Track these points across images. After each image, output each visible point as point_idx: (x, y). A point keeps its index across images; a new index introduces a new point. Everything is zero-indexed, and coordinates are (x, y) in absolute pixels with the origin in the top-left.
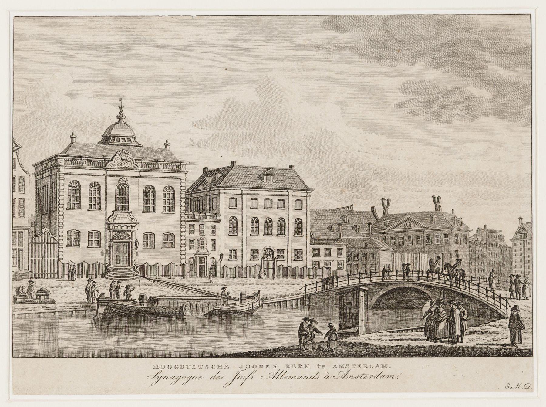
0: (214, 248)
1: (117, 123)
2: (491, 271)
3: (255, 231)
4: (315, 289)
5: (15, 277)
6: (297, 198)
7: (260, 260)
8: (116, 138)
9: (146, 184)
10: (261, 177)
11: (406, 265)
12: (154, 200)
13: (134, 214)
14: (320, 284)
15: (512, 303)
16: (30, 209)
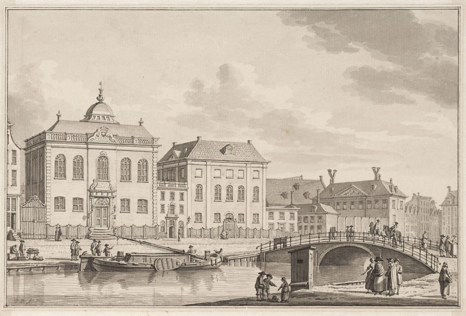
0: (182, 211)
1: (97, 104)
2: (424, 233)
3: (218, 197)
4: (269, 248)
5: (9, 237)
6: (241, 169)
7: (222, 222)
8: (96, 116)
9: (123, 157)
10: (223, 151)
11: (349, 227)
12: (65, 170)
13: (113, 183)
14: (272, 244)
15: (442, 260)
16: (21, 178)
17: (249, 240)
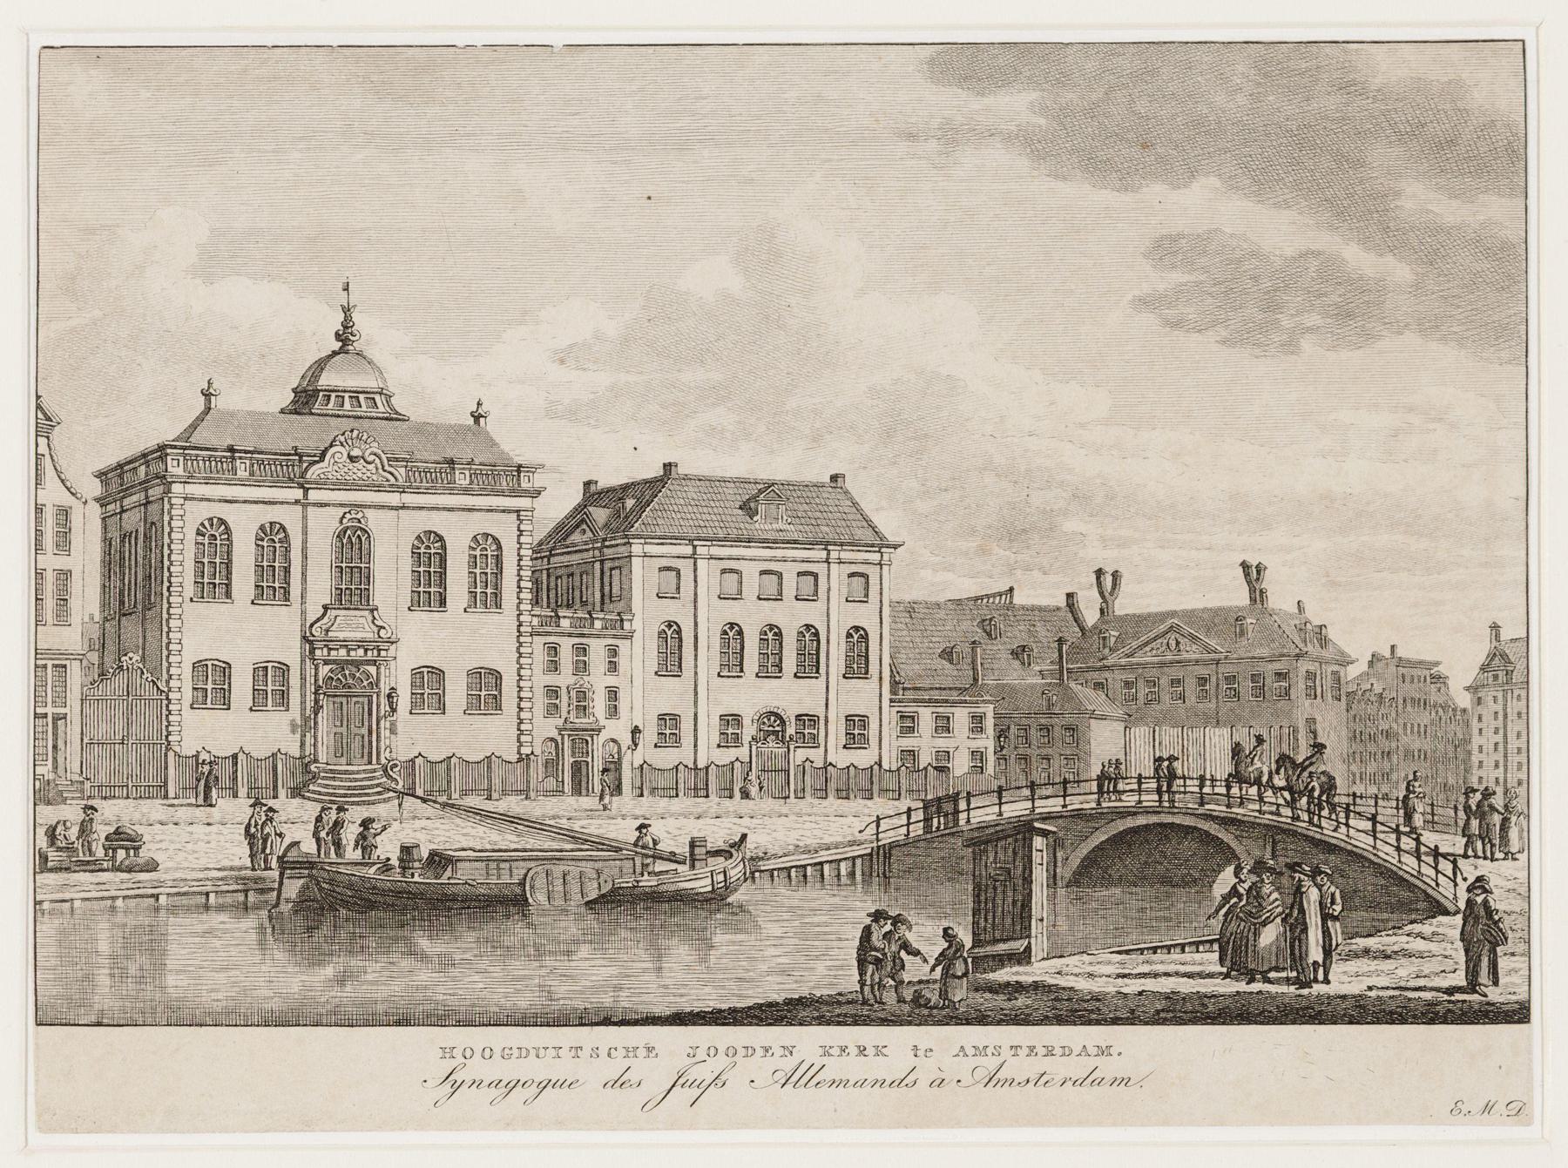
0: (613, 712)
1: (335, 353)
3: (733, 664)
4: (904, 830)
5: (43, 794)
6: (854, 568)
7: (747, 746)
8: (333, 395)
9: (421, 528)
10: (748, 508)
11: (1165, 760)
13: (386, 615)
14: (918, 815)
16: (87, 599)
17: (832, 803)
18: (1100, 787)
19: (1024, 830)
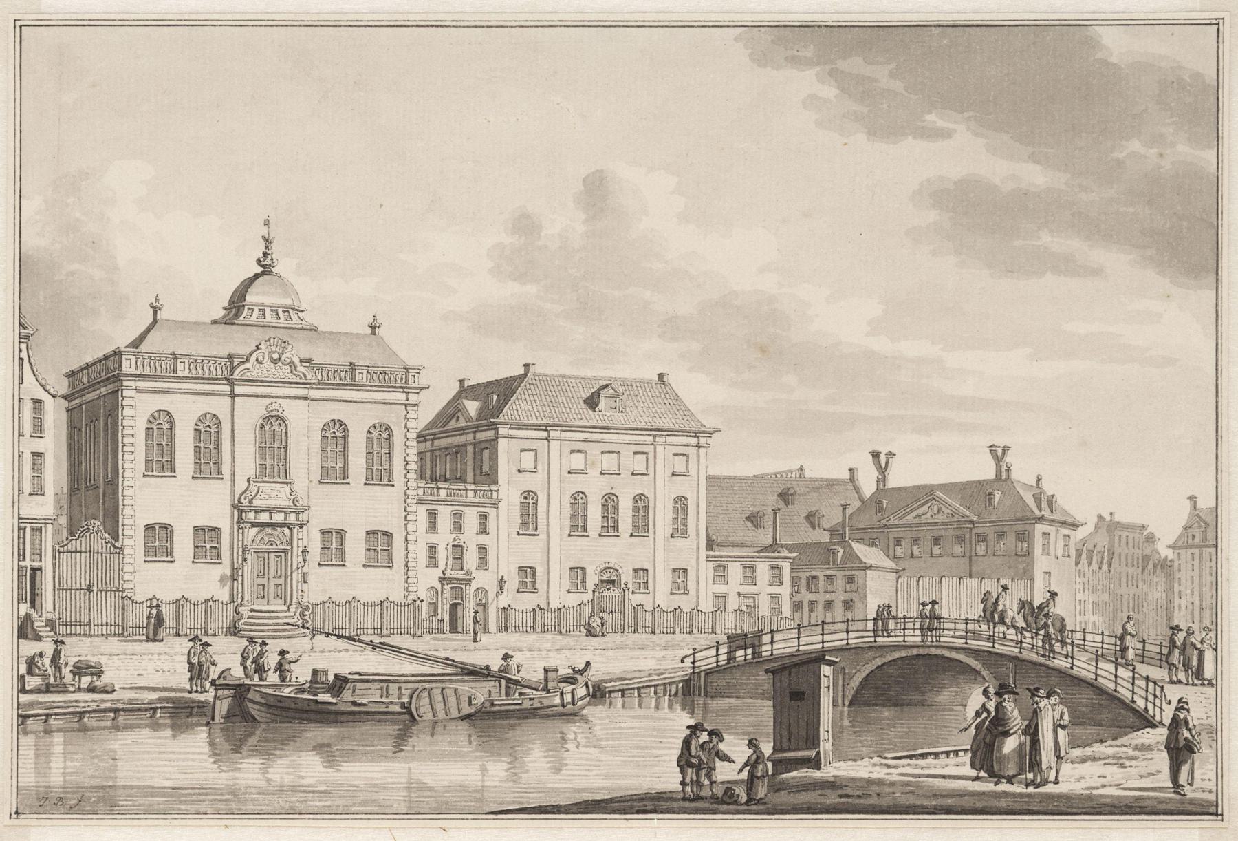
0: (483, 562)
1: (257, 276)
3: (579, 525)
4: (714, 659)
5: (25, 630)
7: (590, 592)
8: (256, 309)
9: (328, 417)
10: (592, 402)
11: (928, 605)
13: (300, 486)
15: (1173, 693)
16: (55, 474)
18: (875, 625)
19: (818, 658)
